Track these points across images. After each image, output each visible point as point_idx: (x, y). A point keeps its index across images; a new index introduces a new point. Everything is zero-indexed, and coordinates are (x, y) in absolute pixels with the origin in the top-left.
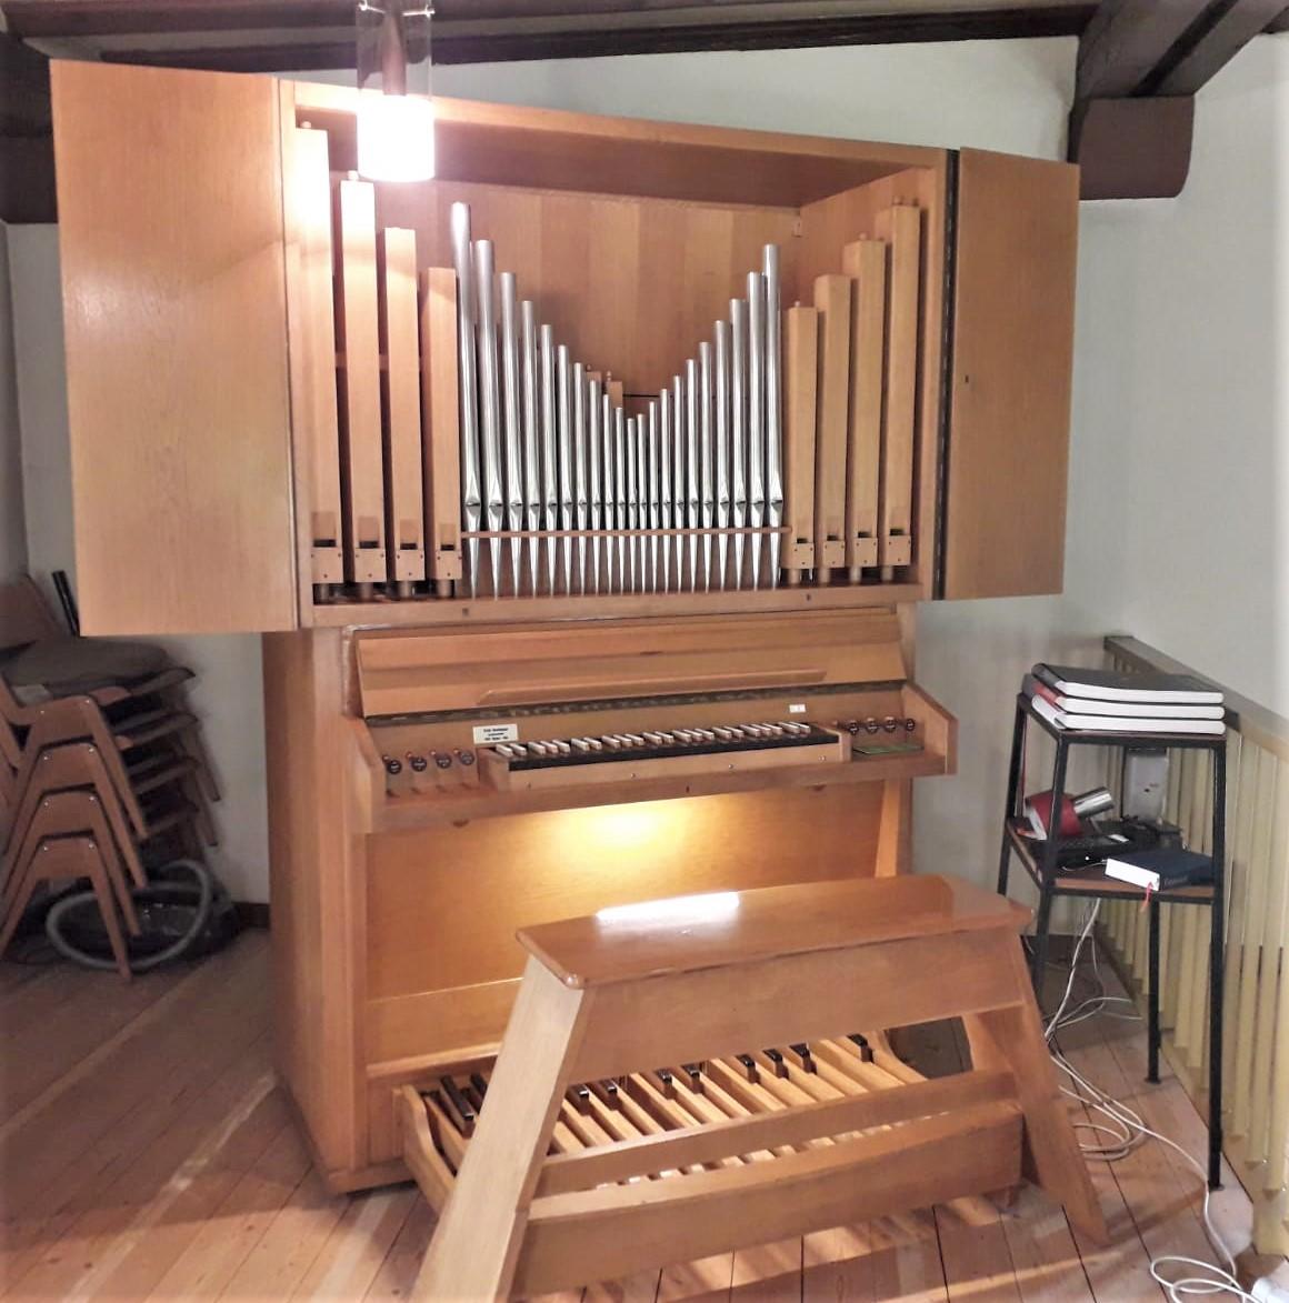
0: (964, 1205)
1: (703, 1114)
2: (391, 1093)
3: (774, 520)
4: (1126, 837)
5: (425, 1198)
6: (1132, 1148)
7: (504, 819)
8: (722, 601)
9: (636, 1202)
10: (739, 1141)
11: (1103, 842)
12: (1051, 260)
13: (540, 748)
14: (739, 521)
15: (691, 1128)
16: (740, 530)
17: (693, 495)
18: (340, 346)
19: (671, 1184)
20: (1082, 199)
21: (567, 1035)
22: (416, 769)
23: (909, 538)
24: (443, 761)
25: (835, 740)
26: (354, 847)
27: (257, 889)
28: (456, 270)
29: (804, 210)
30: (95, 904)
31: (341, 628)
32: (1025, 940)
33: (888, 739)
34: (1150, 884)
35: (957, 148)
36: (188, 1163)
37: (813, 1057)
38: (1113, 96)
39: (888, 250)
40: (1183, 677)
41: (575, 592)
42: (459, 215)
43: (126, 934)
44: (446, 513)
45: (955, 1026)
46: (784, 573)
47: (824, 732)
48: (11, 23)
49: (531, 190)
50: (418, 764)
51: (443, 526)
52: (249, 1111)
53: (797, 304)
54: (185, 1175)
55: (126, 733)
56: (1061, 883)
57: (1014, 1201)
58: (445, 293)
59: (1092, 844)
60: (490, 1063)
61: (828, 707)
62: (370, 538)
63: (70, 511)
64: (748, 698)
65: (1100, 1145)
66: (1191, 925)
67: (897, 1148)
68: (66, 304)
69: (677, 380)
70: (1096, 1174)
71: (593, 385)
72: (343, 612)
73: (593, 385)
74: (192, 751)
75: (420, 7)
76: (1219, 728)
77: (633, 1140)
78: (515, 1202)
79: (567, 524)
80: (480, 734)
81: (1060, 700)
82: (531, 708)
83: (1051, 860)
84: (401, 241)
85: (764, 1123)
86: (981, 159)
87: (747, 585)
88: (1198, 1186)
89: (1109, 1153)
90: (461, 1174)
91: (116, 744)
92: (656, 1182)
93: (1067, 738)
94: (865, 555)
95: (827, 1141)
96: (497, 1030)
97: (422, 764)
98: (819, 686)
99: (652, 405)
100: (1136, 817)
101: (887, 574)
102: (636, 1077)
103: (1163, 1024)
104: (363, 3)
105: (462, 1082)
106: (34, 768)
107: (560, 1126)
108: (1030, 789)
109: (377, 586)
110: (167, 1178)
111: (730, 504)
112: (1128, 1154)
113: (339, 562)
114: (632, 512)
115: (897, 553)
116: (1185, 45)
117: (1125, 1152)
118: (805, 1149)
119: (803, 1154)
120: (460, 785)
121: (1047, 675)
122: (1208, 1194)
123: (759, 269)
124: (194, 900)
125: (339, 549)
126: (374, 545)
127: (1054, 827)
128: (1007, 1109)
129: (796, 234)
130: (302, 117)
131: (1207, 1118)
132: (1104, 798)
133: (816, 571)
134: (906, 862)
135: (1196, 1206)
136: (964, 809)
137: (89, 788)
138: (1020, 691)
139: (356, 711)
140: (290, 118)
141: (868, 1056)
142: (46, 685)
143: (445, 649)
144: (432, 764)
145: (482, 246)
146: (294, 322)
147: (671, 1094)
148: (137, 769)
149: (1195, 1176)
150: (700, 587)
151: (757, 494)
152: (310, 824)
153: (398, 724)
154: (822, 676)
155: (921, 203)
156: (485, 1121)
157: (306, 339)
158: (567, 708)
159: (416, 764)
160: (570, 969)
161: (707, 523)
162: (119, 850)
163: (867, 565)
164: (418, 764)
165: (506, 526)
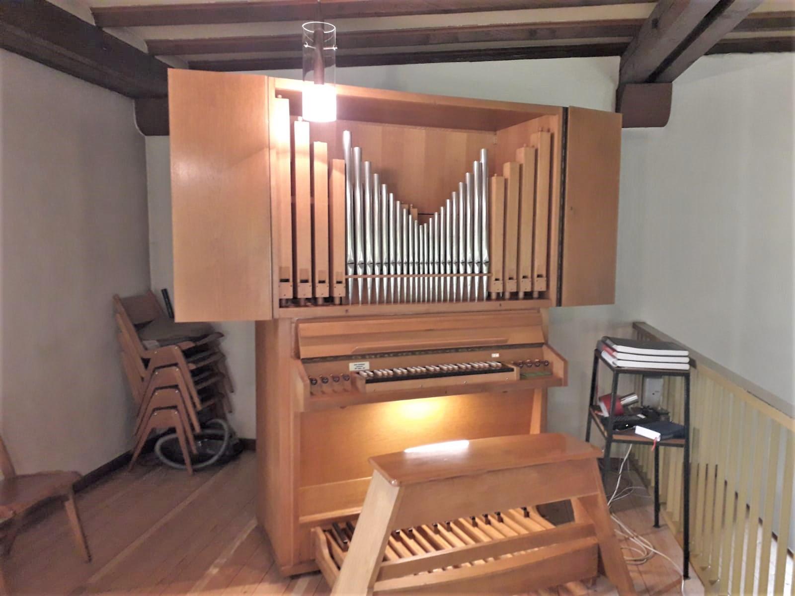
0: (571, 585)
1: (453, 542)
2: (310, 531)
3: (485, 270)
4: (644, 415)
5: (325, 579)
6: (648, 559)
7: (363, 406)
8: (461, 306)
9: (422, 584)
10: (469, 555)
11: (634, 418)
12: (609, 156)
13: (379, 373)
14: (469, 271)
15: (447, 549)
16: (477, 275)
17: (449, 258)
18: (293, 193)
19: (437, 576)
20: (623, 127)
21: (391, 508)
22: (324, 382)
23: (545, 279)
24: (336, 379)
25: (512, 370)
26: (296, 416)
27: (250, 433)
28: (345, 160)
29: (498, 132)
30: (176, 440)
31: (291, 318)
32: (600, 460)
33: (537, 369)
34: (656, 438)
35: (568, 107)
36: (218, 561)
37: (502, 515)
38: (636, 83)
39: (536, 151)
40: (670, 343)
41: (395, 302)
42: (346, 136)
43: (190, 452)
44: (339, 267)
45: (568, 503)
46: (489, 294)
47: (507, 366)
48: (150, 48)
49: (378, 124)
50: (324, 380)
51: (337, 273)
52: (245, 536)
53: (496, 175)
54: (215, 567)
55: (194, 362)
56: (615, 437)
57: (594, 584)
58: (340, 171)
59: (630, 418)
60: (356, 517)
61: (510, 355)
62: (304, 278)
63: (171, 263)
64: (472, 351)
65: (633, 557)
66: (675, 456)
67: (541, 559)
68: (172, 175)
69: (442, 208)
70: (633, 571)
71: (405, 211)
72: (293, 312)
73: (405, 211)
74: (222, 371)
75: (331, 45)
76: (687, 367)
77: (421, 555)
78: (367, 584)
79: (392, 272)
80: (353, 366)
81: (614, 354)
82: (376, 355)
83: (611, 426)
84: (321, 148)
85: (480, 548)
86: (578, 111)
87: (472, 299)
88: (678, 577)
89: (638, 561)
90: (343, 569)
91: (188, 367)
92: (431, 574)
93: (618, 371)
94: (526, 286)
95: (509, 556)
96: (360, 501)
97: (326, 380)
98: (504, 346)
99: (431, 219)
100: (648, 406)
101: (536, 295)
102: (424, 527)
103: (661, 501)
104: (306, 44)
105: (342, 526)
106: (151, 378)
107: (388, 547)
108: (600, 393)
109: (308, 299)
110: (207, 567)
111: (465, 263)
112: (646, 562)
113: (291, 289)
114: (421, 266)
115: (540, 285)
116: (668, 61)
117: (645, 560)
118: (499, 559)
119: (498, 561)
120: (344, 390)
121: (608, 342)
122: (683, 581)
123: (479, 159)
124: (221, 438)
125: (291, 283)
126: (306, 281)
127: (612, 411)
128: (591, 541)
129: (494, 143)
130: (278, 93)
131: (683, 546)
132: (634, 398)
133: (503, 293)
134: (544, 427)
135: (678, 587)
136: (571, 400)
137: (176, 387)
138: (595, 348)
139: (297, 355)
140: (273, 93)
141: (527, 515)
142: (158, 341)
143: (338, 328)
144: (330, 380)
145: (357, 150)
146: (273, 183)
147: (437, 532)
148: (197, 378)
149: (676, 572)
150: (458, 300)
151: (477, 258)
152: (272, 403)
153: (315, 362)
154: (506, 341)
155: (551, 131)
156: (353, 545)
157: (278, 190)
158: (391, 355)
159: (324, 380)
160: (394, 477)
161: (455, 271)
162: (188, 415)
163: (512, 291)
164: (324, 380)
165: (365, 273)
